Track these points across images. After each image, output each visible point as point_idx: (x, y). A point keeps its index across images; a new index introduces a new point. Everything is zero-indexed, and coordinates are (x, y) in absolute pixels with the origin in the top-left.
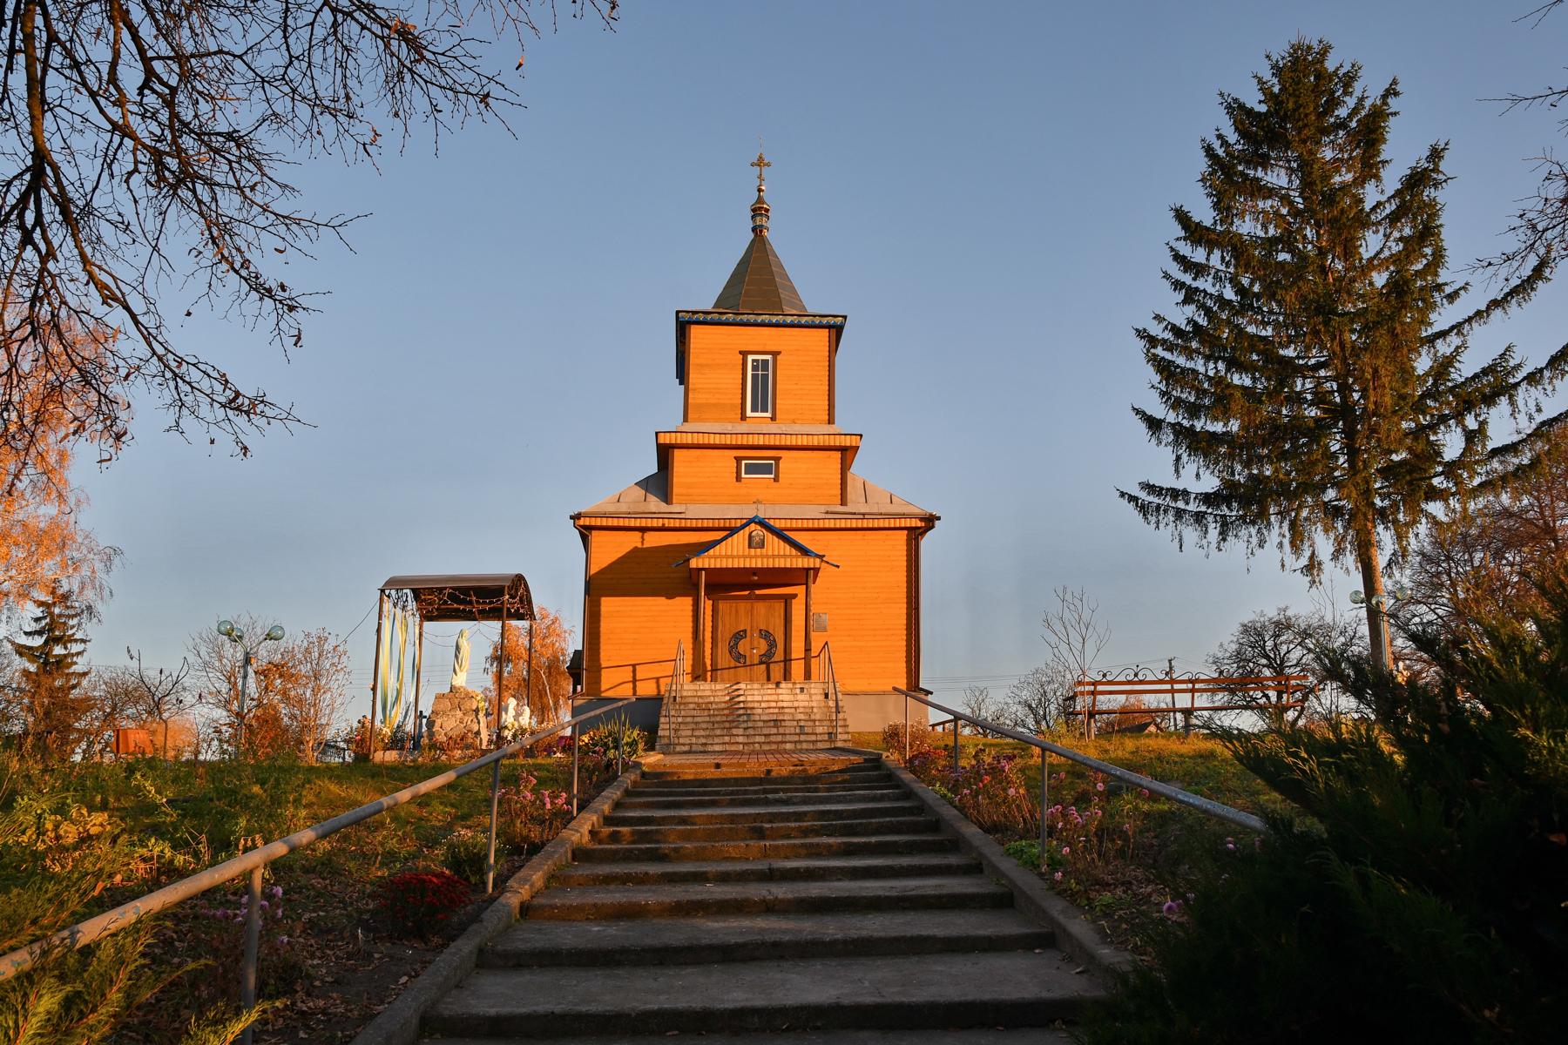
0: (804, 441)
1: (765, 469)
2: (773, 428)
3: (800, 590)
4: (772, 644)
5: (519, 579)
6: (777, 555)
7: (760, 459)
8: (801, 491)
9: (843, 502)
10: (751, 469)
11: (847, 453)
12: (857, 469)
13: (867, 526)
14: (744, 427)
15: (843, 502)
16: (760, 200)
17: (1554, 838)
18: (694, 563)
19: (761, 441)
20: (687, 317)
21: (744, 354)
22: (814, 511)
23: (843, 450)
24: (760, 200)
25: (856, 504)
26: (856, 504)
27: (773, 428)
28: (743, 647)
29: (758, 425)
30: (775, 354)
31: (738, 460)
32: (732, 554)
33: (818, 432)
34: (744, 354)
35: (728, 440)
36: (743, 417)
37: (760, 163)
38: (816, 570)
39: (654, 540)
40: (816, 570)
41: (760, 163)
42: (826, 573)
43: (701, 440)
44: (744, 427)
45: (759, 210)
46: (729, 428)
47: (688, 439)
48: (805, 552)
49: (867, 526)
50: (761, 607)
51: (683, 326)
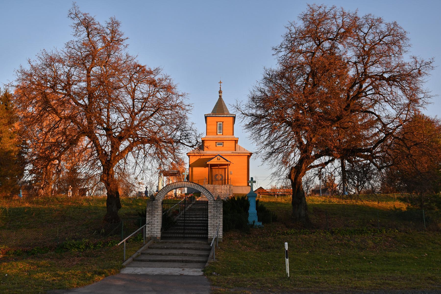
0: (228, 139)
1: (221, 144)
2: (222, 136)
3: (227, 167)
4: (222, 177)
5: (314, 27)
6: (222, 161)
7: (220, 142)
8: (225, 150)
9: (235, 150)
10: (218, 144)
11: (236, 141)
12: (239, 143)
13: (239, 155)
14: (217, 136)
15: (235, 150)
16: (220, 90)
17: (286, 244)
18: (208, 163)
19: (220, 139)
20: (206, 116)
21: (217, 122)
22: (229, 152)
23: (235, 141)
24: (220, 90)
25: (238, 151)
26: (238, 151)
27: (222, 136)
28: (217, 177)
29: (220, 136)
30: (223, 122)
31: (216, 143)
32: (214, 161)
33: (230, 137)
34: (217, 122)
35: (214, 139)
36: (217, 134)
37: (220, 82)
38: (229, 164)
39: (202, 157)
40: (229, 164)
41: (220, 82)
42: (231, 164)
43: (209, 139)
44: (217, 136)
45: (220, 92)
46: (214, 136)
47: (207, 139)
48: (227, 161)
49: (239, 155)
50: (220, 170)
51: (206, 117)
